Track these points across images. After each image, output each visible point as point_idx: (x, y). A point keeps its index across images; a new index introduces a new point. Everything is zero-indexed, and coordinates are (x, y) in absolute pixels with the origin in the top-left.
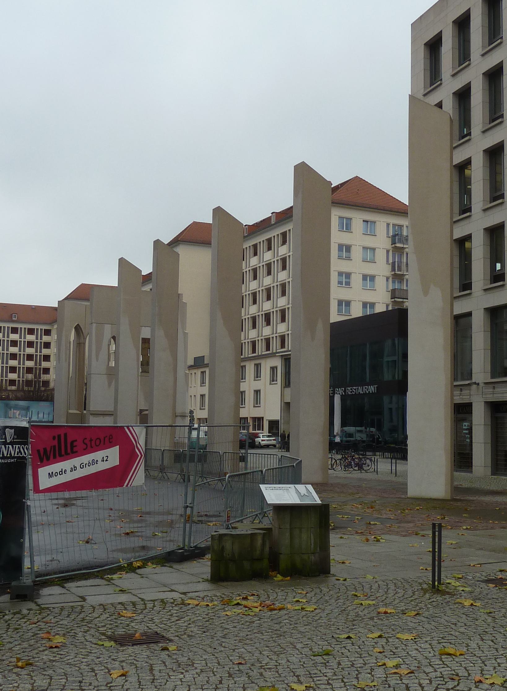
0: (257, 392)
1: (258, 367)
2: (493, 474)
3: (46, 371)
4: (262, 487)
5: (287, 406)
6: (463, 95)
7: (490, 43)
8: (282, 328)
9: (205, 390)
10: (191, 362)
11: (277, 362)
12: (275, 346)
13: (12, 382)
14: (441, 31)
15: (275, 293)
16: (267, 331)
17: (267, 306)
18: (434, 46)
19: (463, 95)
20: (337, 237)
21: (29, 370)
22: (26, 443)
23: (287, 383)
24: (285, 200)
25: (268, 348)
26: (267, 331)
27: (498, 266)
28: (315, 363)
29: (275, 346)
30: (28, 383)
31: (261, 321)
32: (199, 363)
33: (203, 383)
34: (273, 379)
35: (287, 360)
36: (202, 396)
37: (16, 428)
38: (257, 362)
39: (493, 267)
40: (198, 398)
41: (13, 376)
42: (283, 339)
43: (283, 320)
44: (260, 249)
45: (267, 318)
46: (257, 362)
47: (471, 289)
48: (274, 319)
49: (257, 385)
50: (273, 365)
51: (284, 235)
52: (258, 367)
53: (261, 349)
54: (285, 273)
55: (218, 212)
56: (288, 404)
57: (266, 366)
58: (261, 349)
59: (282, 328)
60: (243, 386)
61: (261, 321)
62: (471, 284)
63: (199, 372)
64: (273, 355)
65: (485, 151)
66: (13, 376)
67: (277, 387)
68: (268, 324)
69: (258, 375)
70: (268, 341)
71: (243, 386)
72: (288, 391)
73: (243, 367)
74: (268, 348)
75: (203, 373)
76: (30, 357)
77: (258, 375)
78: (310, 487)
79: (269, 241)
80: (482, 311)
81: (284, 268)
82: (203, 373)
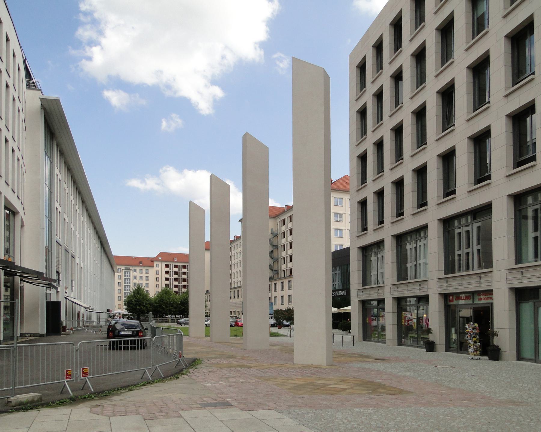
18: (362, 67)
36: (282, 297)
47: (367, 230)
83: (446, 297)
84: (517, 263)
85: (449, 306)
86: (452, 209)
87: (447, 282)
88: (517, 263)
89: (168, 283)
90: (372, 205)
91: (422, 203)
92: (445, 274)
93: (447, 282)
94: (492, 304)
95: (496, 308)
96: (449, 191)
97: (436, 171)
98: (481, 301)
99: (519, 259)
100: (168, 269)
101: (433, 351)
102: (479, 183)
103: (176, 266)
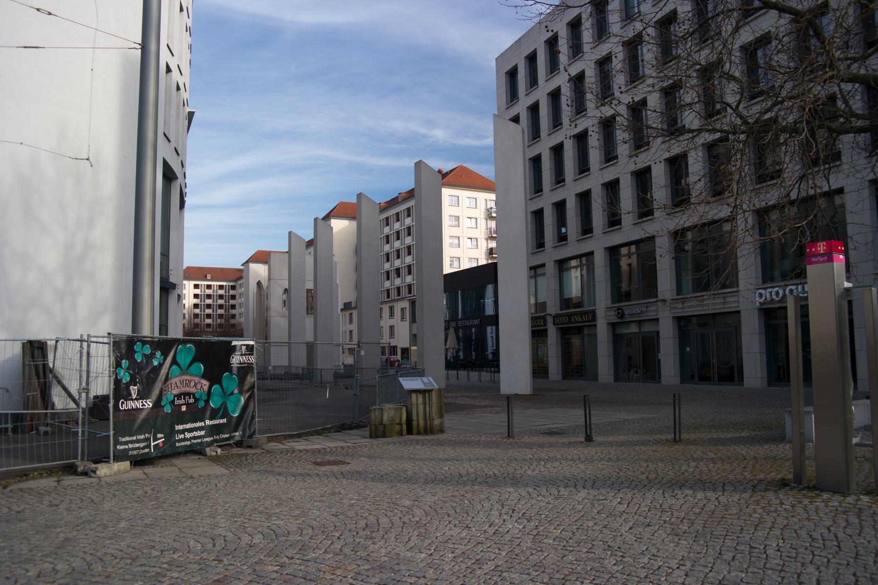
0: (392, 327)
1: (392, 309)
2: (563, 379)
3: (233, 316)
4: (400, 379)
5: (414, 338)
6: (534, 109)
7: (552, 73)
8: (409, 279)
9: (354, 327)
10: (341, 306)
11: (406, 304)
12: (404, 292)
13: (209, 325)
14: (516, 65)
15: (403, 253)
16: (398, 282)
17: (397, 263)
18: (512, 74)
19: (534, 109)
20: (447, 210)
21: (221, 316)
22: (252, 355)
23: (413, 320)
24: (409, 183)
25: (399, 295)
26: (398, 282)
27: (563, 230)
28: (436, 306)
29: (404, 292)
30: (220, 326)
31: (393, 275)
32: (347, 306)
33: (351, 321)
34: (403, 318)
35: (413, 303)
36: (351, 331)
37: (247, 346)
38: (391, 304)
39: (559, 231)
40: (348, 333)
41: (209, 321)
42: (410, 286)
43: (410, 273)
44: (391, 221)
45: (398, 272)
46: (391, 304)
47: (567, 240)
48: (403, 272)
49: (392, 322)
50: (403, 306)
51: (408, 209)
52: (392, 309)
53: (393, 294)
54: (410, 238)
55: (359, 196)
56: (415, 335)
57: (398, 306)
58: (393, 294)
59: (409, 279)
60: (382, 323)
61: (393, 275)
62: (592, 228)
63: (347, 313)
64: (403, 299)
65: (550, 148)
66: (209, 321)
67: (407, 323)
68: (399, 276)
69: (392, 315)
70: (399, 289)
71: (382, 323)
72: (414, 325)
73: (381, 309)
74: (399, 295)
75: (351, 314)
76: (221, 307)
77: (392, 315)
78: (431, 379)
79: (397, 214)
80: (553, 263)
81: (409, 254)
82: (351, 314)
83: (678, 319)
84: (678, 295)
85: (622, 336)
86: (616, 239)
87: (683, 303)
88: (678, 295)
89: (197, 311)
90: (600, 201)
91: (587, 230)
92: (613, 303)
93: (683, 303)
94: (658, 333)
95: (662, 335)
96: (614, 221)
97: (630, 189)
98: (648, 328)
99: (679, 290)
100: (198, 291)
101: (31, 342)
102: (612, 226)
103: (209, 287)
